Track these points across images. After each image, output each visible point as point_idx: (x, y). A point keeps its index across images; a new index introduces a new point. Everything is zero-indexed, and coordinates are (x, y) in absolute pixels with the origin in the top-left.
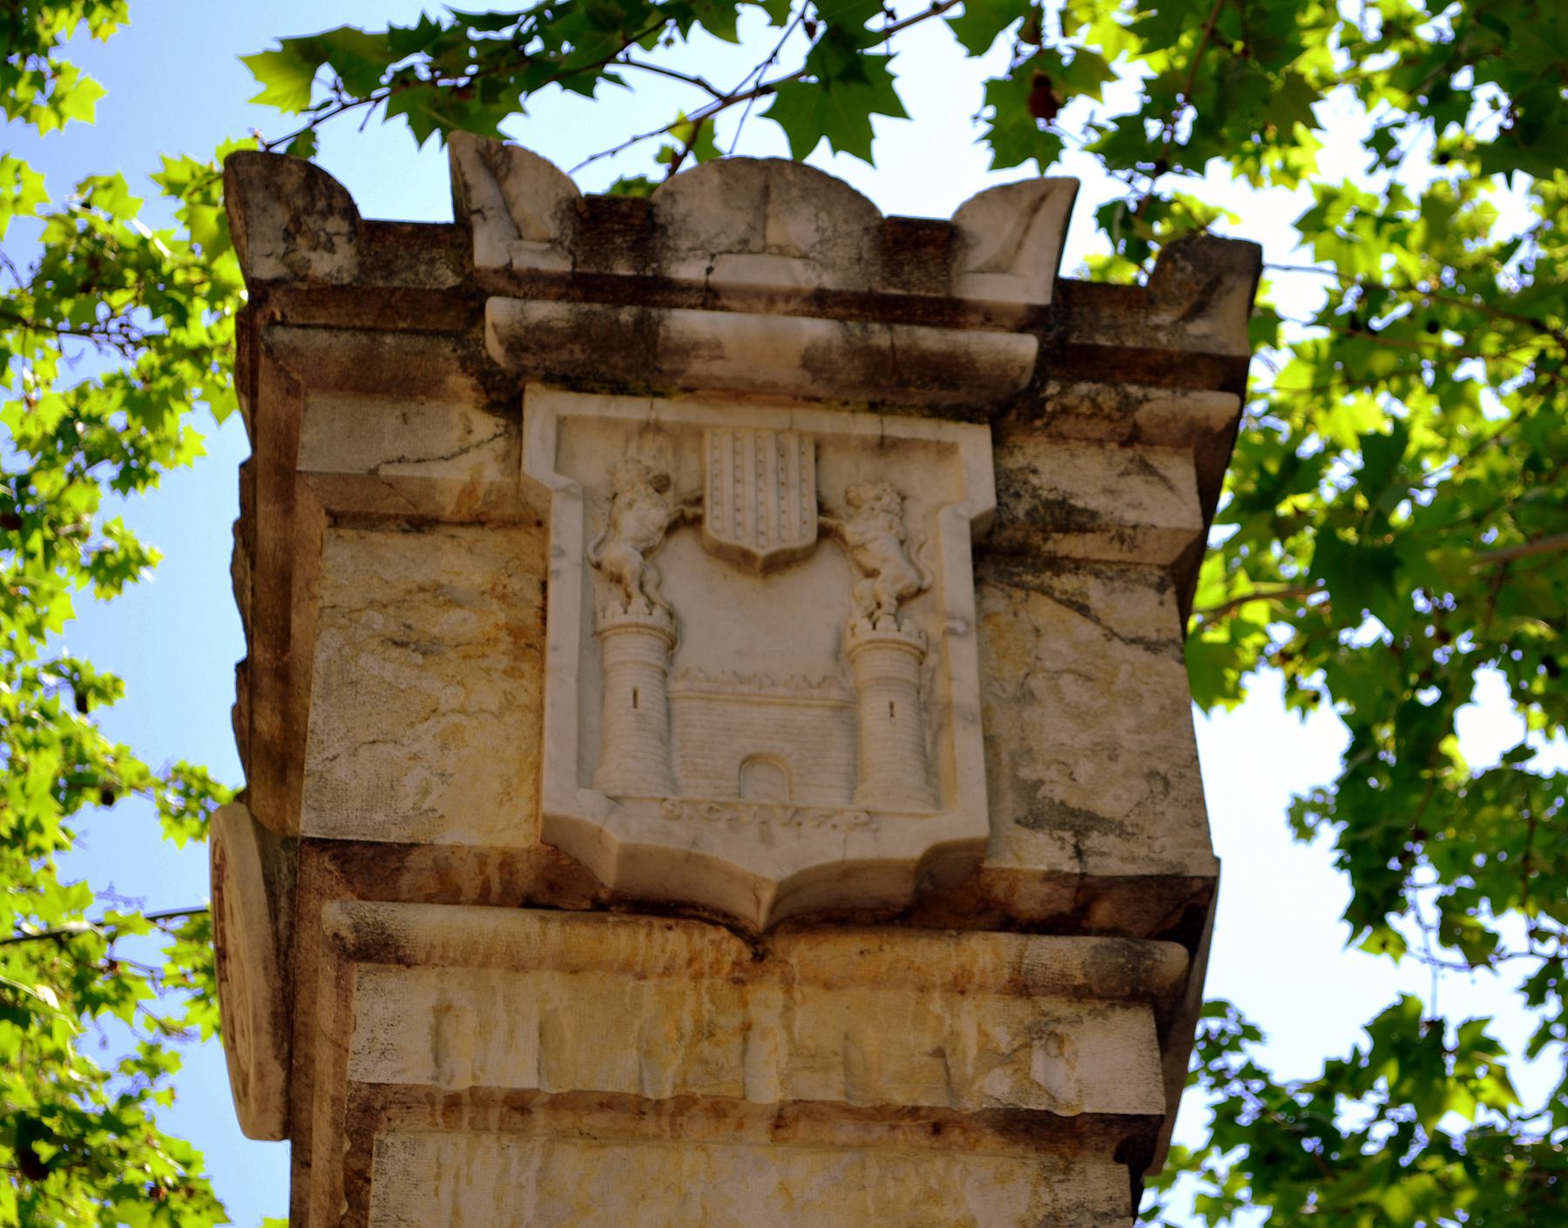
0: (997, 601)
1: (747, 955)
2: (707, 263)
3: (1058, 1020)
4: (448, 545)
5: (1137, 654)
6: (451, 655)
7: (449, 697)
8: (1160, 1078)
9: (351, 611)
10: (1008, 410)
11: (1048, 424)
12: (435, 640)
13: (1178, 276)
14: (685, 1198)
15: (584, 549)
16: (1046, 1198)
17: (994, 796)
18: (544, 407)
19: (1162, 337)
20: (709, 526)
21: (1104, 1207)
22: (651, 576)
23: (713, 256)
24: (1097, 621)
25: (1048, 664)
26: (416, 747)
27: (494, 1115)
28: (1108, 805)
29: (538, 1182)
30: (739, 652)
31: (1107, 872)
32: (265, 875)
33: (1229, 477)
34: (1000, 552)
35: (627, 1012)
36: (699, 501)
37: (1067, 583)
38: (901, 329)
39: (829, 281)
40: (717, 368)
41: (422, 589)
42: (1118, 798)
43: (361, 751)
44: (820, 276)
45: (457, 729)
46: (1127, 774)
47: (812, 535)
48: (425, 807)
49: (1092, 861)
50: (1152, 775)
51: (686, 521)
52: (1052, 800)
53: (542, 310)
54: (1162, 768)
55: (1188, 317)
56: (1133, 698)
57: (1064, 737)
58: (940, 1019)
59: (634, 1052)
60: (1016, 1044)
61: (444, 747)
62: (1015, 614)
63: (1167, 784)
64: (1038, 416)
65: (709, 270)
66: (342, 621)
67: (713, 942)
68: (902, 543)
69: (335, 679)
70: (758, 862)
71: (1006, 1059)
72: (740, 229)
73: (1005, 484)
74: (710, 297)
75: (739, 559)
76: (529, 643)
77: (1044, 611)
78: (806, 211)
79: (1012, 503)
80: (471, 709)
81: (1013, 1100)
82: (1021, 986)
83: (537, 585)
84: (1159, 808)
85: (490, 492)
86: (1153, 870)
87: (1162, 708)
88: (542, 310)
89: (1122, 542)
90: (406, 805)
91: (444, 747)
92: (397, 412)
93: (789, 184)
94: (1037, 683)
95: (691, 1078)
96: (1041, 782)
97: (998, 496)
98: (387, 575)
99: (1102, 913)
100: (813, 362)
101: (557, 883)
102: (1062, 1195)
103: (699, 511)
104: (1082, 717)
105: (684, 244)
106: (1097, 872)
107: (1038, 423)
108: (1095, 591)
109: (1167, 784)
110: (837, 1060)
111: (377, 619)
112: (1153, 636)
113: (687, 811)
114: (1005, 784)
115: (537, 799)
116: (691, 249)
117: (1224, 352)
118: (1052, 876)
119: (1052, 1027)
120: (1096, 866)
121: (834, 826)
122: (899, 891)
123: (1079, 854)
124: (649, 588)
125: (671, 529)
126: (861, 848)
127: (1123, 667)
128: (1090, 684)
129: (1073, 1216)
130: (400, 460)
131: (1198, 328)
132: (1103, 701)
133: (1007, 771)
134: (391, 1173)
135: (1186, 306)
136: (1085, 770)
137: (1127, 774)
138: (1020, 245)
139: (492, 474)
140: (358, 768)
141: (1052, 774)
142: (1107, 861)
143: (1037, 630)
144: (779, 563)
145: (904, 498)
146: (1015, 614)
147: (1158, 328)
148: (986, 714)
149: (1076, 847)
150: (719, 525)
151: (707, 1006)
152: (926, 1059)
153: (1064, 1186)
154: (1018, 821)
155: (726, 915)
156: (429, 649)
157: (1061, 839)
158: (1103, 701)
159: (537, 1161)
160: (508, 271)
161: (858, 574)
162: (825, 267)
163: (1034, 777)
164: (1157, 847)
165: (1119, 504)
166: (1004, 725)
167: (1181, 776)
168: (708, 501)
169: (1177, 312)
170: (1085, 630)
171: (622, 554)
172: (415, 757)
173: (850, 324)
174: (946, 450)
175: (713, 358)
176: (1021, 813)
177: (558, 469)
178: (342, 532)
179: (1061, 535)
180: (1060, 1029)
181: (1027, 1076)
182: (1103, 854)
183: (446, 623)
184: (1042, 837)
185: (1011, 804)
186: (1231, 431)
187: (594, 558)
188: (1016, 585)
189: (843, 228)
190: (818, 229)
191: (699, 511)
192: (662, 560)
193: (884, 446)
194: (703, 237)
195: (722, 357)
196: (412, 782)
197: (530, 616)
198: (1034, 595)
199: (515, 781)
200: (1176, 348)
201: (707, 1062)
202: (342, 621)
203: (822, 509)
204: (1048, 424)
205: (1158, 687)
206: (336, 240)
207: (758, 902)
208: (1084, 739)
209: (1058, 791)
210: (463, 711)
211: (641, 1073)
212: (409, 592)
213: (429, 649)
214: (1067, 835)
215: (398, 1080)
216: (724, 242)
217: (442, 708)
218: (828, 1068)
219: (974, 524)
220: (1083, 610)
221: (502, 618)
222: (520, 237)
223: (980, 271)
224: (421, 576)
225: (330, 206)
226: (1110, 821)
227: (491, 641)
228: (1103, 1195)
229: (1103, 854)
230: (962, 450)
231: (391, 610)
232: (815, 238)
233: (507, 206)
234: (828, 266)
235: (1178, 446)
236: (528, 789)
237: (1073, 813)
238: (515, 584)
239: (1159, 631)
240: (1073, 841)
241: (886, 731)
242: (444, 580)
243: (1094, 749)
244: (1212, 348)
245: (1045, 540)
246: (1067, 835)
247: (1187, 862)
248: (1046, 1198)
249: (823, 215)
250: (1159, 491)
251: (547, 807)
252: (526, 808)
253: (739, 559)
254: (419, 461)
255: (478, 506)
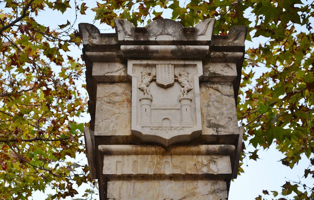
0: (204, 90)
1: (164, 151)
2: (155, 37)
3: (214, 159)
4: (117, 86)
5: (226, 97)
6: (117, 104)
7: (117, 111)
8: (231, 167)
9: (102, 98)
10: (206, 58)
11: (212, 60)
12: (115, 102)
13: (233, 33)
14: (156, 190)
15: (137, 86)
16: (213, 188)
17: (203, 122)
18: (130, 63)
19: (230, 44)
20: (157, 81)
21: (222, 189)
22: (148, 90)
23: (156, 36)
24: (220, 92)
25: (212, 100)
26: (112, 120)
27: (126, 178)
28: (221, 123)
29: (133, 189)
30: (162, 101)
31: (221, 134)
32: (91, 139)
33: (223, 145)
34: (203, 81)
35: (145, 164)
36: (155, 77)
37: (215, 86)
38: (186, 46)
39: (175, 39)
40: (157, 55)
41: (112, 94)
42: (223, 122)
43: (103, 121)
44: (173, 38)
45: (118, 116)
46: (225, 117)
47: (173, 81)
48: (114, 129)
49: (219, 133)
50: (229, 118)
51: (154, 80)
52: (213, 123)
53: (129, 47)
54: (230, 116)
55: (235, 40)
56: (226, 105)
57: (215, 112)
58: (195, 159)
59: (147, 167)
60: (208, 163)
61: (116, 119)
62: (207, 92)
63: (231, 119)
64: (210, 59)
65: (156, 39)
66: (100, 100)
67: (159, 149)
68: (188, 81)
69: (99, 109)
70: (167, 135)
71: (206, 165)
72: (161, 31)
73: (204, 70)
74: (156, 43)
75: (161, 86)
76: (130, 101)
77: (211, 91)
78: (171, 27)
79: (206, 73)
80: (120, 113)
81: (207, 172)
82: (208, 153)
83: (130, 92)
84: (230, 123)
85: (122, 77)
86: (229, 134)
87: (231, 106)
88: (129, 47)
89: (224, 78)
90: (111, 129)
91: (116, 119)
92: (108, 65)
93: (168, 23)
94: (210, 103)
95: (156, 171)
96: (211, 120)
97: (203, 72)
98: (107, 92)
99: (221, 140)
100: (173, 52)
101: (135, 139)
102: (215, 187)
103: (155, 78)
104: (217, 109)
105: (152, 34)
106: (220, 134)
107: (210, 60)
108: (220, 87)
109: (231, 119)
110: (179, 167)
111: (105, 99)
112: (229, 94)
113: (154, 128)
114: (205, 121)
115: (131, 127)
116: (153, 35)
117: (240, 46)
118: (213, 135)
119: (213, 160)
120: (220, 133)
121: (177, 130)
122: (189, 139)
123: (217, 131)
124: (147, 92)
125: (151, 82)
126: (182, 133)
127: (224, 100)
128: (219, 103)
129: (217, 191)
130: (108, 73)
131: (236, 42)
132: (221, 106)
133: (205, 118)
134: (110, 188)
135: (234, 38)
136: (218, 117)
137: (225, 117)
138: (206, 30)
139: (123, 74)
140: (103, 124)
141: (213, 118)
142: (222, 132)
143: (210, 94)
144: (170, 86)
145: (188, 74)
146: (207, 92)
147: (229, 42)
148: (201, 109)
149: (216, 130)
150: (159, 81)
151: (159, 159)
152: (193, 166)
153: (216, 186)
154: (207, 127)
155: (161, 144)
156: (114, 103)
157: (214, 129)
158: (221, 106)
159: (132, 186)
160: (124, 41)
161: (181, 87)
162: (174, 37)
163: (210, 119)
164: (230, 130)
165: (223, 72)
166: (205, 110)
167: (234, 117)
168: (157, 77)
169: (233, 39)
170: (218, 94)
171: (143, 86)
172: (112, 121)
173: (179, 46)
174: (195, 65)
175: (157, 53)
176: (207, 125)
177: (133, 73)
178: (100, 85)
179: (214, 78)
180: (215, 160)
181: (209, 168)
182: (221, 131)
183: (117, 99)
184: (211, 129)
185: (206, 124)
186: (243, 58)
187: (139, 87)
188: (207, 87)
189: (177, 30)
190: (173, 30)
191: (155, 78)
192: (150, 87)
193: (185, 66)
194: (155, 33)
195: (158, 53)
196: (111, 126)
197: (129, 97)
198: (210, 88)
199: (128, 124)
200: (232, 45)
201: (159, 168)
202: (100, 100)
203: (175, 77)
204: (212, 60)
205: (230, 103)
206: (97, 37)
207: (166, 142)
208: (218, 112)
209: (214, 121)
210: (119, 113)
211: (148, 170)
212: (111, 94)
213: (114, 103)
214: (215, 128)
215: (111, 173)
216: (158, 34)
217: (116, 113)
218: (178, 168)
219: (199, 77)
220: (218, 90)
221: (125, 98)
222: (126, 35)
223: (199, 35)
224: (112, 91)
225: (95, 32)
226: (222, 126)
227: (123, 102)
228: (222, 187)
229: (221, 131)
230: (197, 65)
231: (108, 97)
232: (173, 32)
233: (124, 29)
234: (175, 36)
235: (233, 62)
236: (129, 126)
237: (216, 125)
238: (127, 92)
239: (230, 93)
240: (216, 129)
241: (187, 114)
242: (116, 92)
243: (220, 114)
244: (238, 45)
245: (212, 79)
246: (215, 128)
247: (235, 132)
248: (213, 188)
249: (174, 28)
250: (230, 69)
251: (133, 129)
252: (129, 129)
253: (161, 86)
254: (111, 73)
255: (121, 79)
